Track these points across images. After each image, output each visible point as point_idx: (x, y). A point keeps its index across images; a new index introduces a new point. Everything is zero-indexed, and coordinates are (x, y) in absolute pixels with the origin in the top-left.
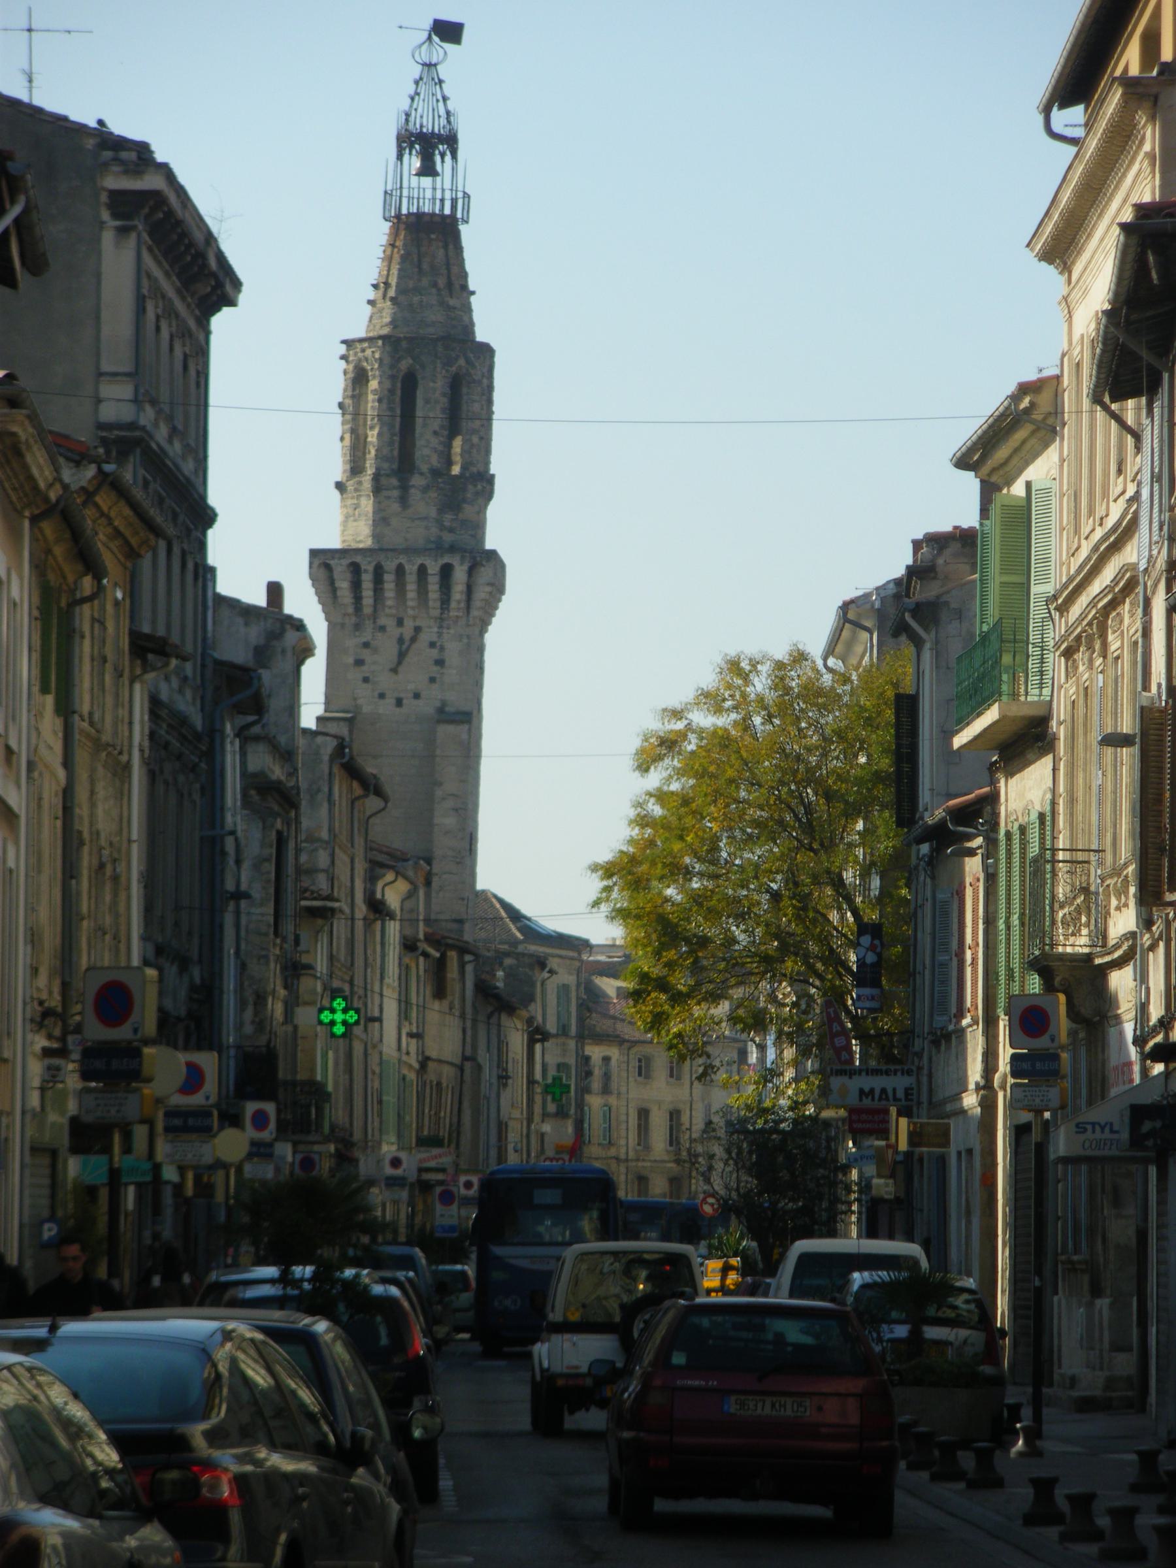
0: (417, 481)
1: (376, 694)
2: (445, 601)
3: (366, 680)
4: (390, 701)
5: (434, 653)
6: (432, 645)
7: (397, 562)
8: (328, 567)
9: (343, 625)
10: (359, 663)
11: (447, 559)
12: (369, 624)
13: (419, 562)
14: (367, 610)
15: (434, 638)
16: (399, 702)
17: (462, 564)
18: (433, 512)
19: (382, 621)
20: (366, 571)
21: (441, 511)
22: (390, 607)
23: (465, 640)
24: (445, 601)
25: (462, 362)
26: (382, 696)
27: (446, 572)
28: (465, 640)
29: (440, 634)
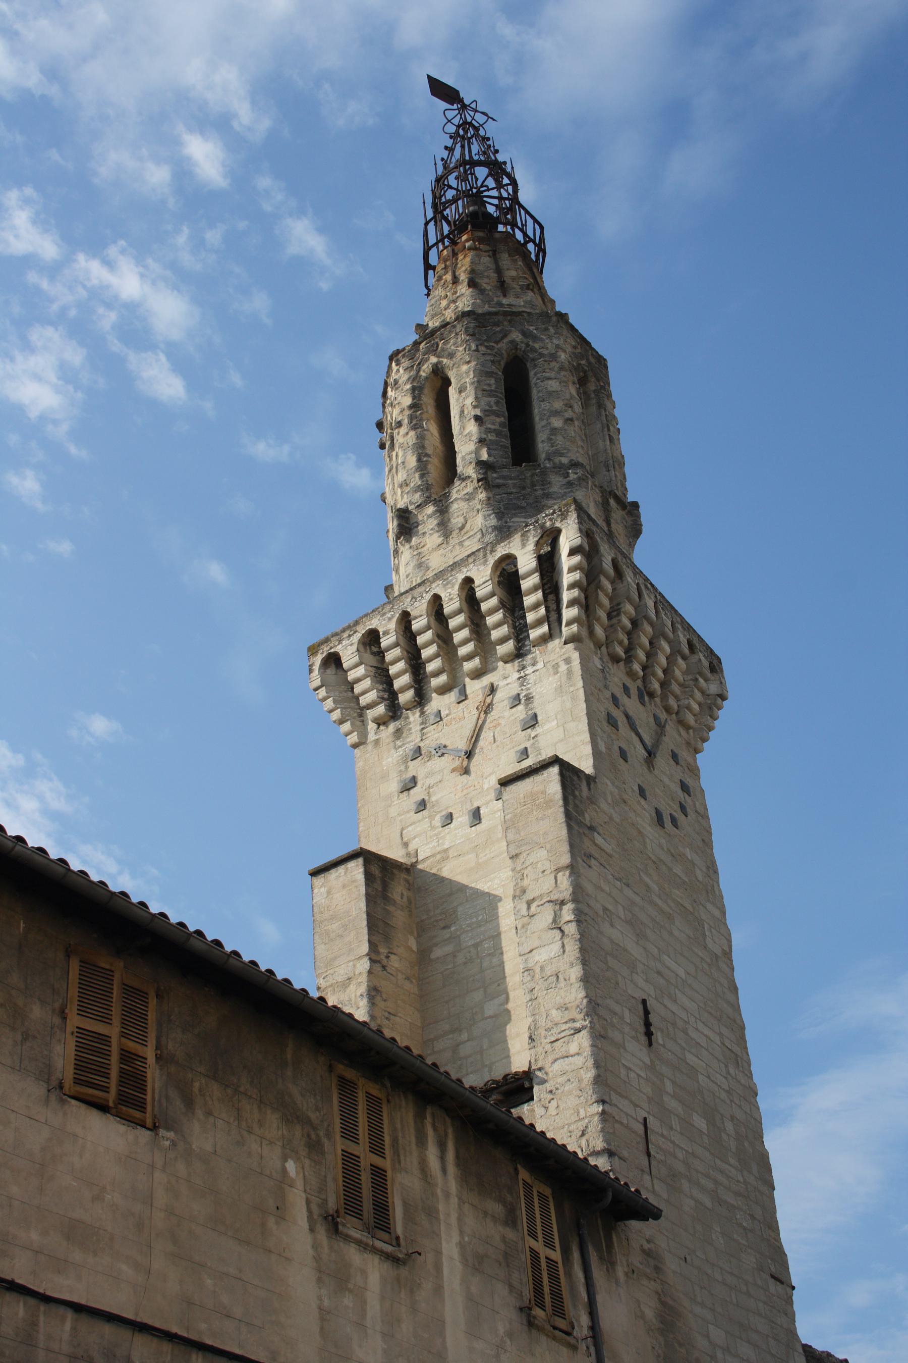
0: (458, 491)
4: (462, 819)
8: (333, 661)
10: (409, 785)
11: (501, 551)
13: (460, 577)
15: (515, 689)
16: (476, 815)
17: (524, 545)
20: (386, 633)
25: (516, 336)
28: (563, 667)
29: (522, 679)
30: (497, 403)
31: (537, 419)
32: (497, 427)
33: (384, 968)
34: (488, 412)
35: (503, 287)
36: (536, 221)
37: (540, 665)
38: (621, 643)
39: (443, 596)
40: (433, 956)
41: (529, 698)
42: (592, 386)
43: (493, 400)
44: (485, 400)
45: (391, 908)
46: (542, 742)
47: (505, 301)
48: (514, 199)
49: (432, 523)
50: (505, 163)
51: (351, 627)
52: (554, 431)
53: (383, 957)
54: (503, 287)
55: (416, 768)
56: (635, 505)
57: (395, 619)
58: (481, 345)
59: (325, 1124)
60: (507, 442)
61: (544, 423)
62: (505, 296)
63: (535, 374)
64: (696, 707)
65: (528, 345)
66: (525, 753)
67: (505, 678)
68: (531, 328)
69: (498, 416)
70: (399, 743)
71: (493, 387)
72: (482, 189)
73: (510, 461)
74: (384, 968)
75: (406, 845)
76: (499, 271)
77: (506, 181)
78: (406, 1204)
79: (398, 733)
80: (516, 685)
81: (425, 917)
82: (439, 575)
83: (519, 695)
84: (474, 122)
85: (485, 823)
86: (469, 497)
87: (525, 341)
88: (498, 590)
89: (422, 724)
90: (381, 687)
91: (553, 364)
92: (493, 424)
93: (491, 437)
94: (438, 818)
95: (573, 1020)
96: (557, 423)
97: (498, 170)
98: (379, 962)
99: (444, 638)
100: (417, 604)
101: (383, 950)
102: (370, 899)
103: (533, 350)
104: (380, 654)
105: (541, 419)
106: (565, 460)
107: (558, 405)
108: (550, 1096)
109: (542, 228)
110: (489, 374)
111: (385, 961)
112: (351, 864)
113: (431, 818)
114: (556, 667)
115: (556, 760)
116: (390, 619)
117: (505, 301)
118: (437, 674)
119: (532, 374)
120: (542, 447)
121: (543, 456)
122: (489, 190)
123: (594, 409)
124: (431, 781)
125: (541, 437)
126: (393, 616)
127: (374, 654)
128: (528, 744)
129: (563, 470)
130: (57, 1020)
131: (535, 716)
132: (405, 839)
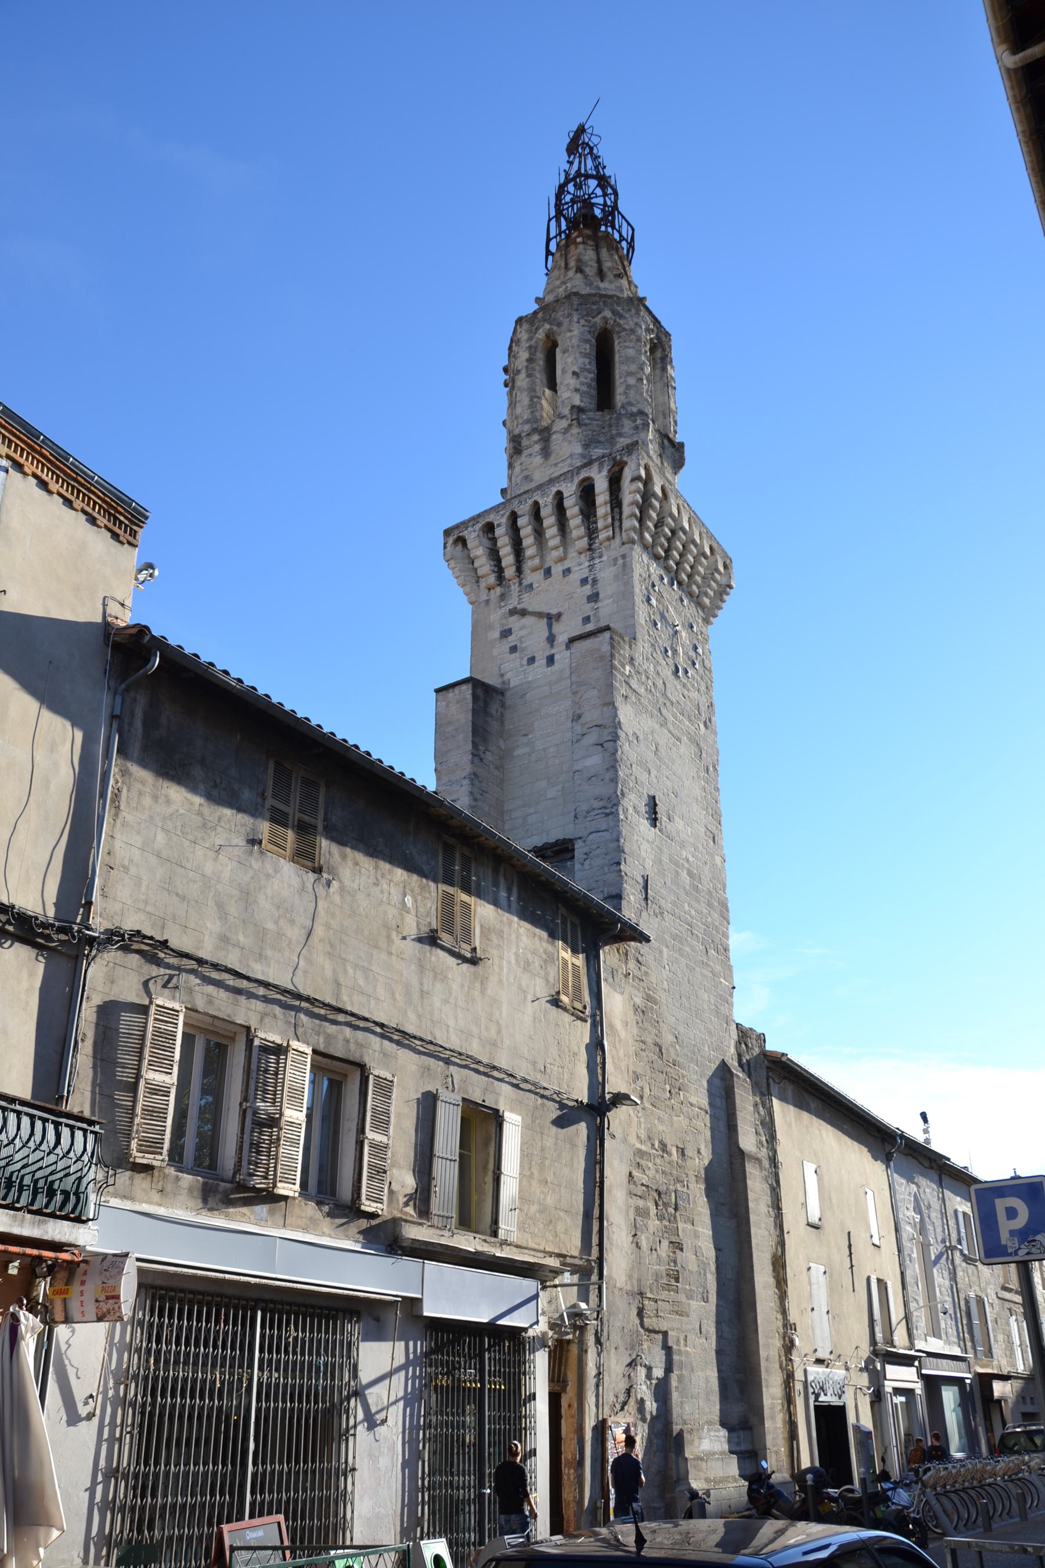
1: (525, 662)
2: (592, 533)
3: (514, 649)
5: (587, 589)
6: (584, 581)
7: (530, 502)
8: (462, 541)
9: (487, 602)
10: (506, 633)
11: (584, 474)
12: (515, 587)
13: (554, 490)
14: (510, 572)
15: (585, 573)
17: (600, 471)
18: (578, 449)
19: (529, 577)
21: (586, 446)
22: (532, 558)
23: (620, 562)
24: (592, 533)
25: (607, 313)
26: (532, 660)
27: (587, 492)
29: (591, 567)
30: (590, 363)
31: (617, 377)
32: (588, 381)
33: (481, 760)
34: (583, 370)
35: (601, 274)
36: (629, 224)
37: (605, 558)
38: (662, 546)
39: (540, 502)
40: (515, 754)
41: (595, 581)
42: (659, 354)
43: (587, 361)
44: (581, 360)
45: (489, 719)
46: (602, 613)
47: (602, 285)
48: (615, 207)
49: (537, 447)
50: (610, 177)
51: (475, 519)
52: (628, 387)
53: (481, 752)
54: (601, 274)
55: (514, 622)
56: (682, 445)
57: (506, 516)
58: (582, 318)
59: (433, 873)
60: (594, 392)
61: (622, 380)
62: (602, 281)
63: (619, 343)
64: (711, 593)
65: (615, 321)
66: (587, 620)
67: (580, 565)
68: (619, 308)
69: (590, 372)
70: (502, 604)
71: (588, 351)
72: (592, 196)
73: (593, 406)
74: (481, 760)
75: (502, 675)
76: (599, 262)
77: (610, 191)
78: (482, 926)
79: (503, 597)
80: (587, 570)
81: (511, 727)
82: (540, 487)
83: (587, 578)
84: (590, 143)
85: (557, 666)
86: (566, 431)
87: (614, 318)
88: (580, 502)
89: (519, 592)
90: (492, 563)
91: (632, 337)
92: (586, 378)
93: (584, 388)
94: (525, 659)
95: (605, 808)
96: (632, 381)
97: (603, 181)
98: (478, 756)
99: (539, 533)
100: (522, 507)
101: (482, 748)
102: (474, 712)
103: (619, 325)
104: (494, 540)
105: (620, 377)
106: (635, 410)
107: (633, 367)
108: (585, 857)
109: (633, 230)
110: (587, 341)
111: (482, 756)
112: (464, 687)
113: (522, 659)
114: (615, 560)
115: (607, 628)
116: (502, 515)
117: (602, 285)
118: (532, 558)
119: (616, 343)
120: (619, 399)
121: (619, 405)
122: (597, 197)
123: (658, 371)
124: (522, 633)
125: (619, 390)
126: (504, 514)
127: (489, 539)
128: (591, 614)
129: (632, 416)
130: (259, 800)
131: (597, 595)
132: (502, 672)
